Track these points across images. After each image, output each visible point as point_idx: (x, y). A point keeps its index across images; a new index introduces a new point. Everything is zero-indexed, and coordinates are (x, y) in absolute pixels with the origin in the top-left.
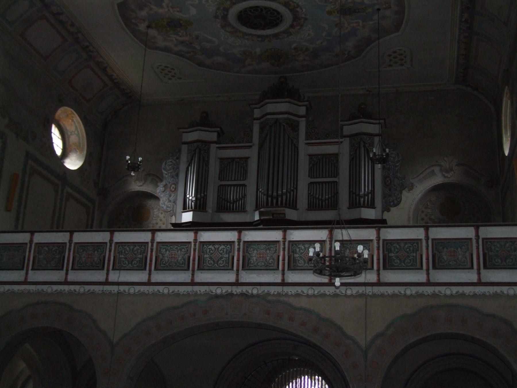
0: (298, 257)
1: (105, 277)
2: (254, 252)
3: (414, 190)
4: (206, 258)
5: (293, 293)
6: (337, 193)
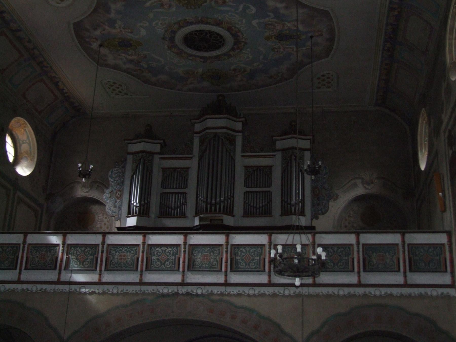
0: (155, 259)
1: (57, 277)
2: (199, 254)
3: (338, 200)
4: (154, 259)
5: (235, 293)
6: (270, 202)
